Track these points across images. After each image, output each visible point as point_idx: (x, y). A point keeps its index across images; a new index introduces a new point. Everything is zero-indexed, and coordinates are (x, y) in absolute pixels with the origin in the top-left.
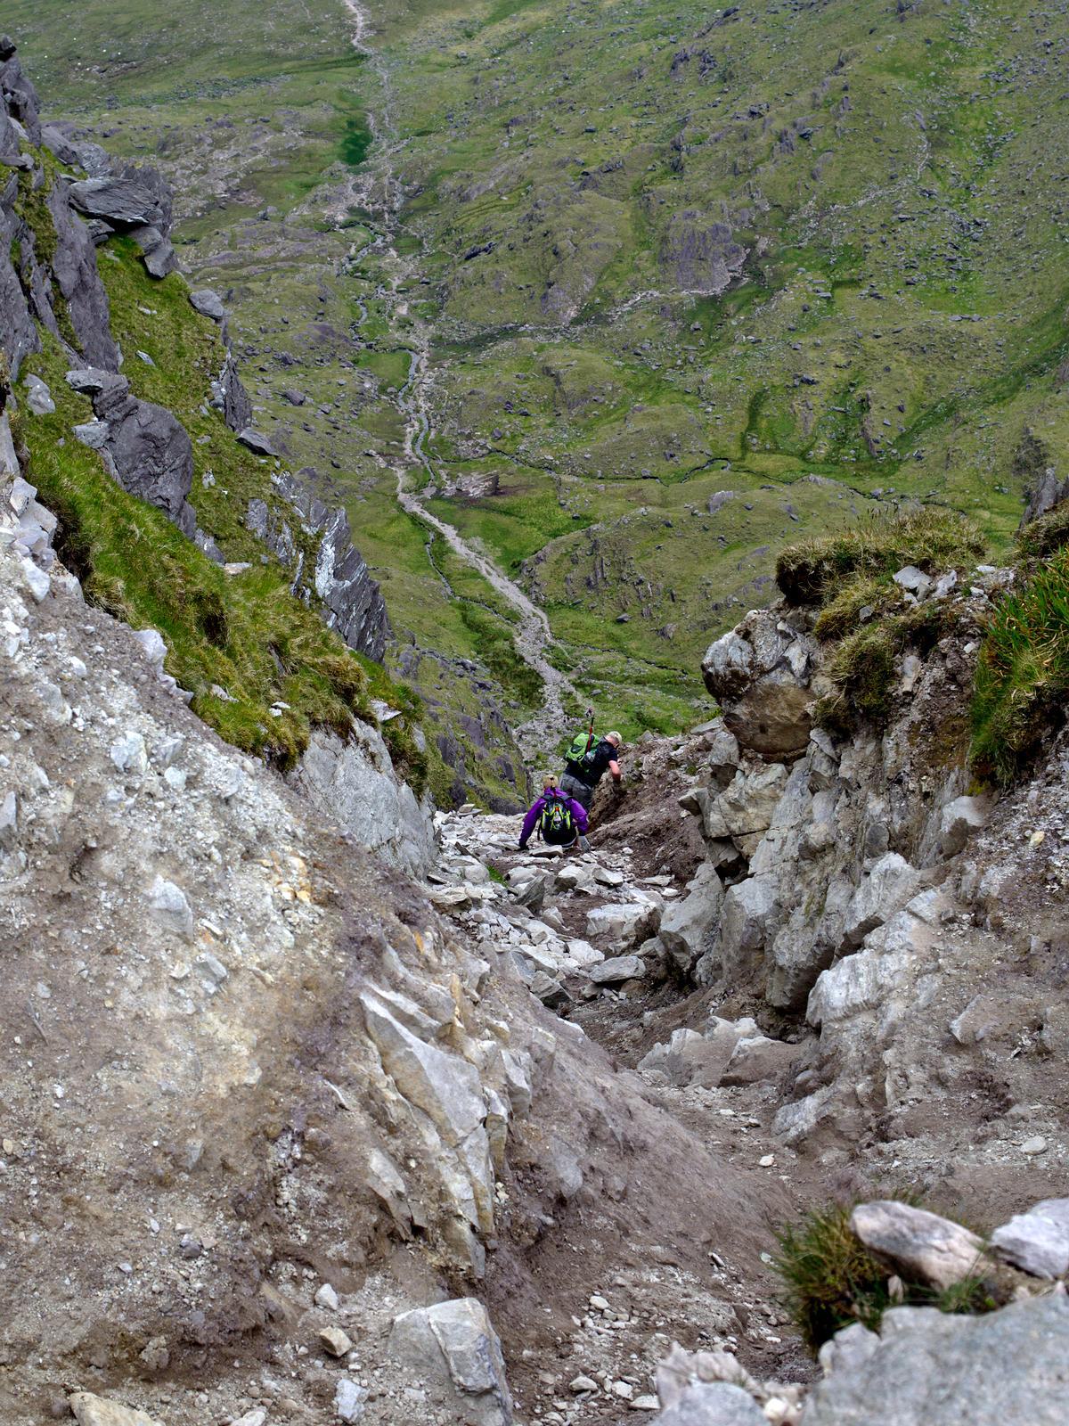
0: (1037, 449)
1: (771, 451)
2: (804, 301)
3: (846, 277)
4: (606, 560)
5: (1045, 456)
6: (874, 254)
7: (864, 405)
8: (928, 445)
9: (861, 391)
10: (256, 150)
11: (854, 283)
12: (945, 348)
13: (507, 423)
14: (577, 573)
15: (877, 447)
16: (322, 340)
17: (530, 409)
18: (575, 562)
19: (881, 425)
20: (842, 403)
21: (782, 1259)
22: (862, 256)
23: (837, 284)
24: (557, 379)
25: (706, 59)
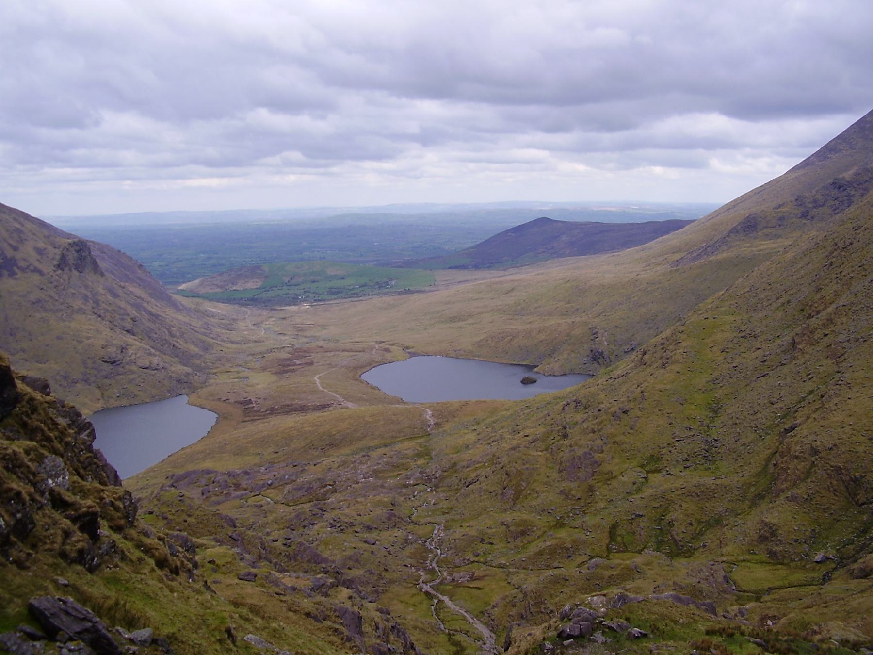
0: (771, 528)
1: (624, 551)
2: (633, 480)
3: (653, 468)
4: (532, 602)
5: (777, 530)
6: (665, 457)
7: (671, 524)
8: (710, 538)
9: (668, 517)
10: (379, 464)
11: (658, 471)
12: (703, 495)
13: (482, 548)
14: (513, 611)
15: (680, 544)
16: (389, 519)
17: (493, 541)
18: (514, 606)
19: (679, 531)
20: (659, 525)
21: (212, 388)
22: (659, 459)
23: (648, 472)
24: (508, 527)
25: (577, 402)
